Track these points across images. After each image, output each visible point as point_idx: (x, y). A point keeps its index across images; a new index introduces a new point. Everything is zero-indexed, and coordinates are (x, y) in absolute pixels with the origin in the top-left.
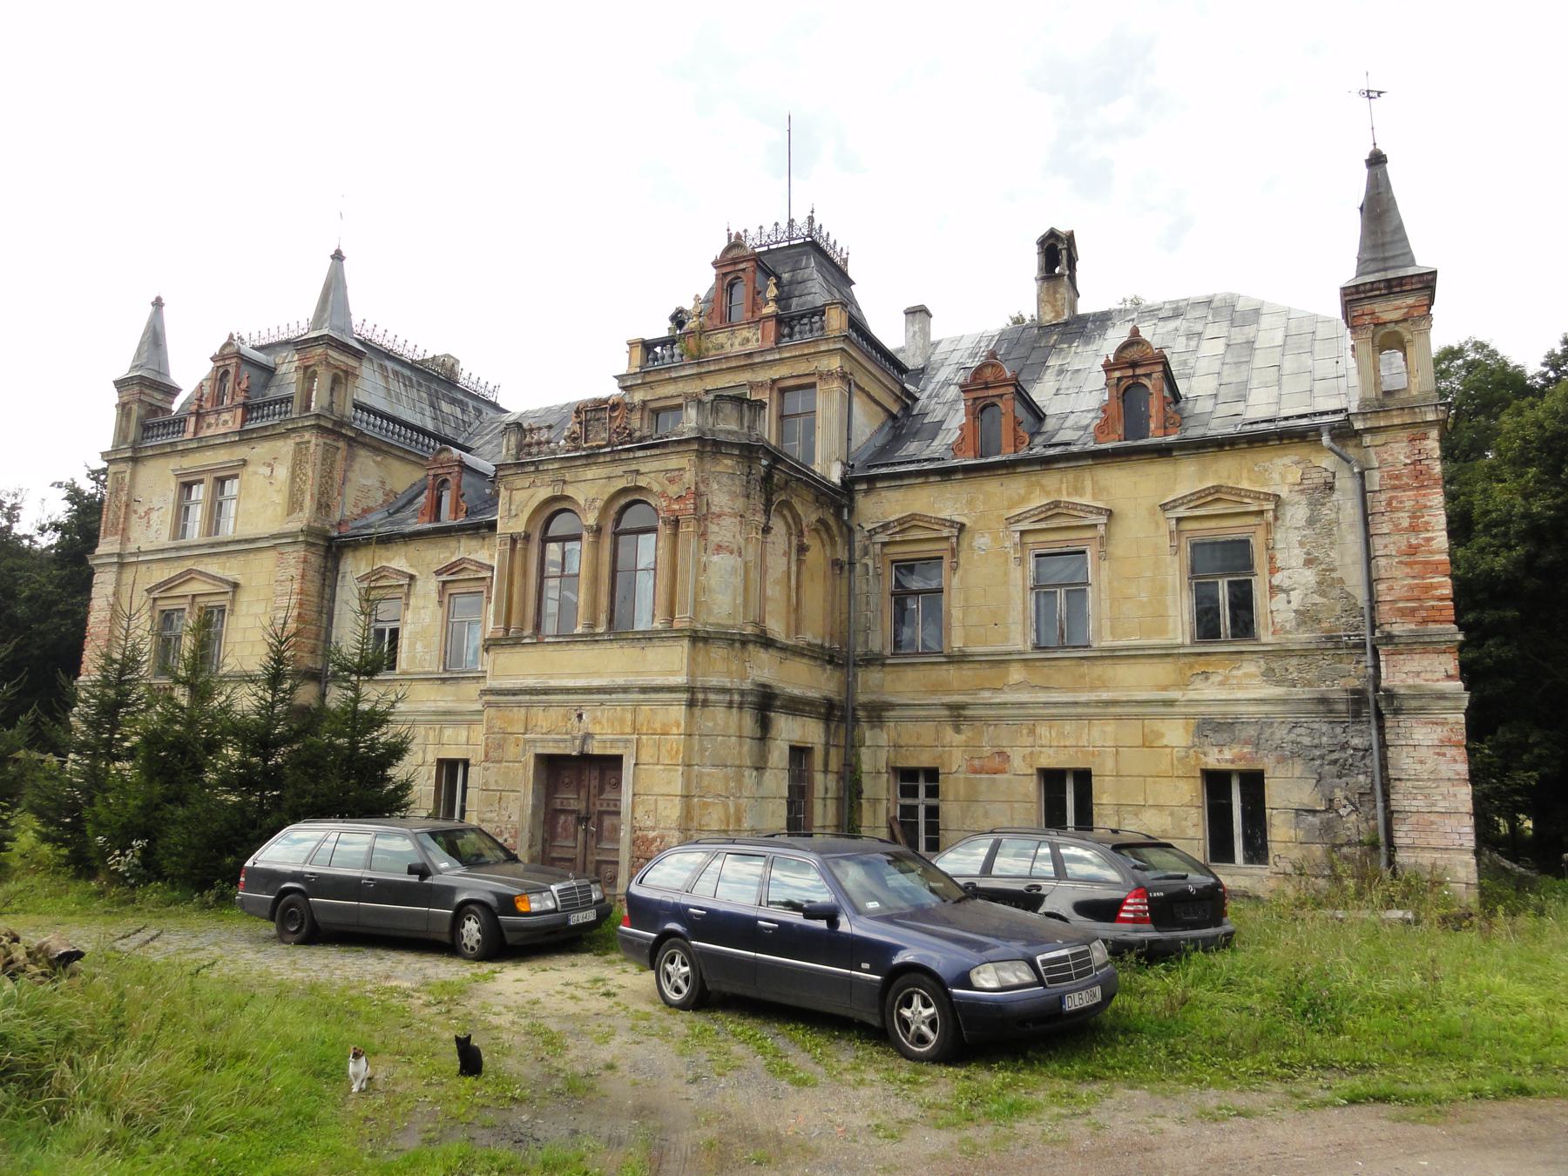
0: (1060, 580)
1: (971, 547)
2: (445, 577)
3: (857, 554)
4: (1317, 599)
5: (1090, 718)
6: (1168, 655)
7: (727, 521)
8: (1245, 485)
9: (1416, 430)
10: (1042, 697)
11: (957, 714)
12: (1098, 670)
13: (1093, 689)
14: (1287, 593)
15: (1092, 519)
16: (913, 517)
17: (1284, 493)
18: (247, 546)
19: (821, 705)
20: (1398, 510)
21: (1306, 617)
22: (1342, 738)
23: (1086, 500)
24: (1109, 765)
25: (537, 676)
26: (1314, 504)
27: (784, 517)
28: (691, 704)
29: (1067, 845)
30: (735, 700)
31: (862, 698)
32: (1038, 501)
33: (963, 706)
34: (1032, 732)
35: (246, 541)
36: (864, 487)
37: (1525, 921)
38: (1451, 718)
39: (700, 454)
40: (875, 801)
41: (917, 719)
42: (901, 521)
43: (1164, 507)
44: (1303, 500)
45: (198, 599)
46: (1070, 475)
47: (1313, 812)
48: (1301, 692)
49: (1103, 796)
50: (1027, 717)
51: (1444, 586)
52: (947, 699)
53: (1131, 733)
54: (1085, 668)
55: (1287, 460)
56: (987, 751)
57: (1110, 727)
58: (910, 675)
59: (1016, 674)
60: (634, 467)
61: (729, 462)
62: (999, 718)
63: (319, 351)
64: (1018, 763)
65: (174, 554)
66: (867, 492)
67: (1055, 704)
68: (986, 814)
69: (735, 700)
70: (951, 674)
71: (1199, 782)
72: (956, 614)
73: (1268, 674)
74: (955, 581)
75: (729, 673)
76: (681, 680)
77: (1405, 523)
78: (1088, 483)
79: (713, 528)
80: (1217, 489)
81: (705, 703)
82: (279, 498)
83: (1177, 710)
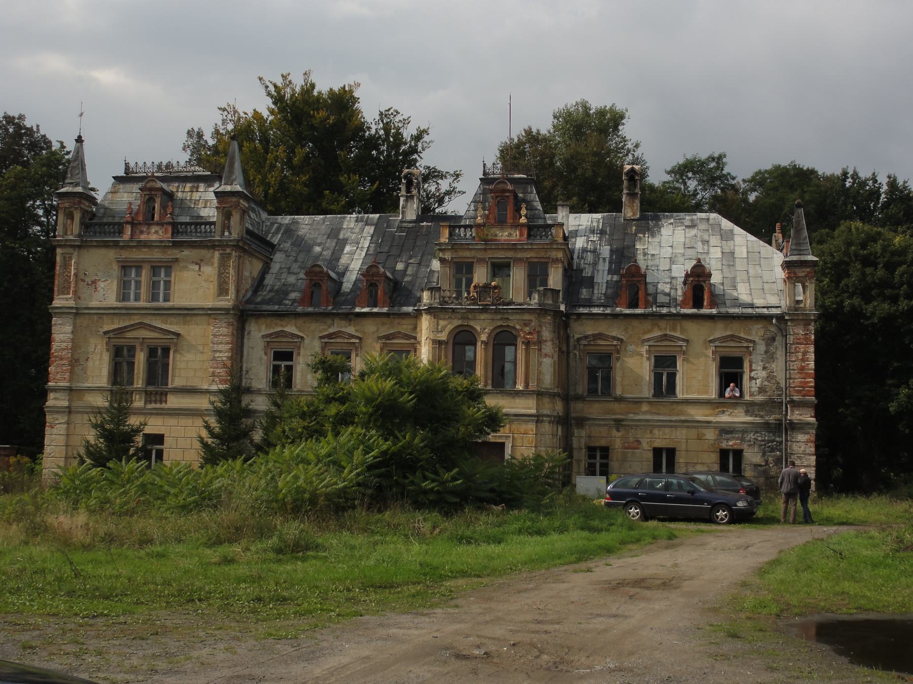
0: (665, 365)
1: (625, 350)
2: (326, 340)
3: (571, 348)
4: (766, 383)
5: (676, 427)
8: (742, 335)
9: (807, 323)
10: (656, 417)
11: (618, 424)
12: (680, 407)
13: (678, 415)
14: (755, 378)
15: (681, 343)
16: (600, 334)
17: (757, 339)
18: (187, 313)
20: (798, 352)
21: (762, 390)
22: (773, 438)
23: (677, 334)
24: (683, 447)
26: (767, 345)
28: (537, 422)
29: (461, 483)
31: (573, 415)
32: (657, 333)
33: (622, 420)
34: (651, 432)
35: (186, 309)
36: (575, 317)
38: (811, 431)
39: (539, 315)
40: (579, 461)
41: (600, 425)
42: (594, 335)
43: (710, 341)
44: (763, 343)
45: (146, 341)
46: (671, 322)
47: (761, 466)
48: (758, 420)
49: (680, 459)
50: (650, 426)
51: (811, 382)
52: (614, 417)
53: (693, 433)
54: (675, 406)
55: (759, 326)
56: (631, 439)
57: (684, 431)
58: (596, 406)
59: (645, 407)
60: (506, 316)
62: (637, 426)
63: (234, 199)
64: (645, 445)
65: (124, 312)
66: (576, 320)
67: (662, 421)
68: (630, 467)
70: (616, 406)
72: (618, 379)
73: (747, 412)
74: (618, 365)
76: (534, 411)
77: (800, 357)
78: (679, 327)
79: (544, 346)
80: (732, 336)
81: (542, 421)
82: (213, 287)
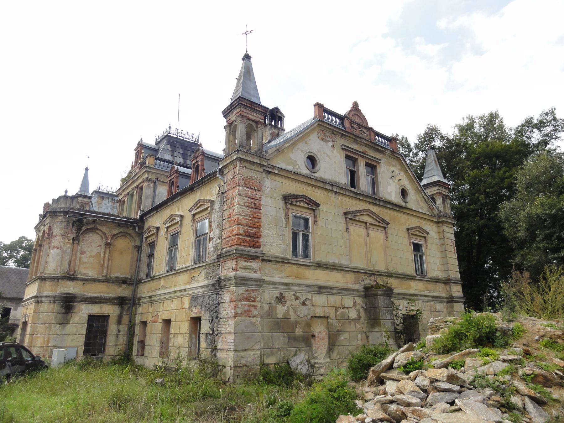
6: (187, 270)
7: (58, 238)
19: (117, 299)
25: (112, 293)
27: (98, 233)
30: (54, 299)
37: (34, 380)
61: (61, 218)
69: (54, 299)
71: (189, 322)
75: (51, 291)
79: (53, 241)
81: (42, 302)
83: (187, 293)
